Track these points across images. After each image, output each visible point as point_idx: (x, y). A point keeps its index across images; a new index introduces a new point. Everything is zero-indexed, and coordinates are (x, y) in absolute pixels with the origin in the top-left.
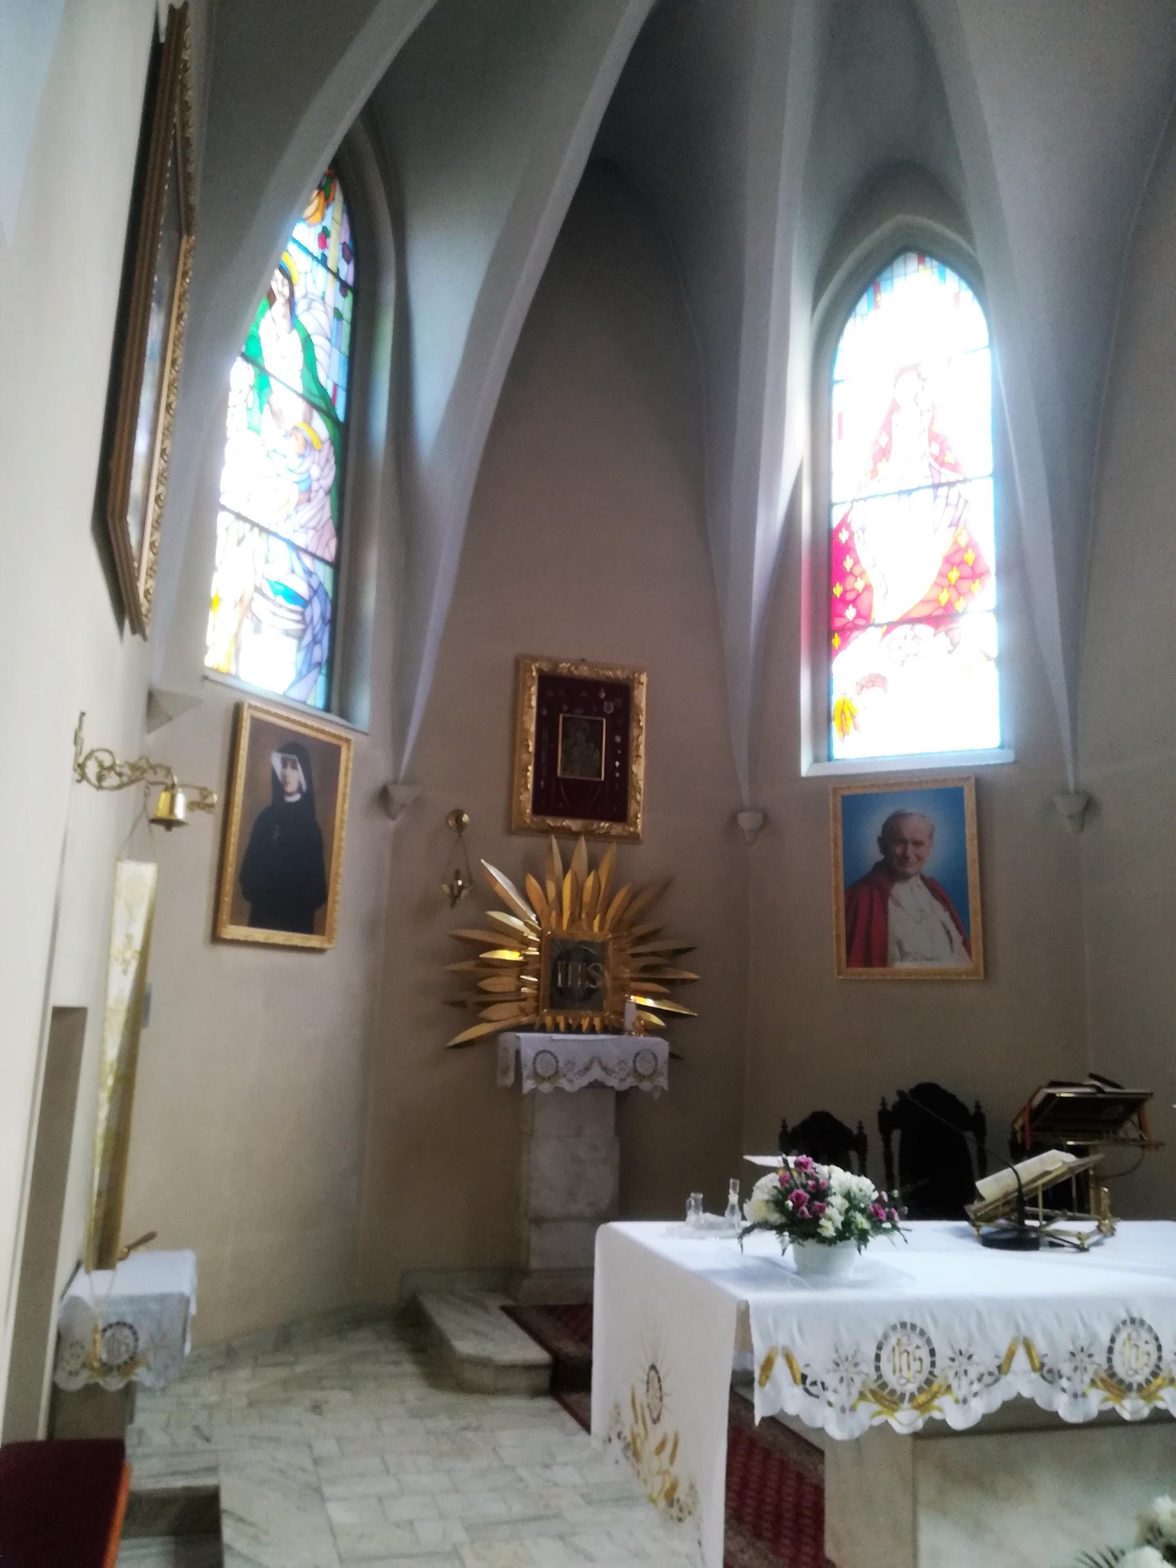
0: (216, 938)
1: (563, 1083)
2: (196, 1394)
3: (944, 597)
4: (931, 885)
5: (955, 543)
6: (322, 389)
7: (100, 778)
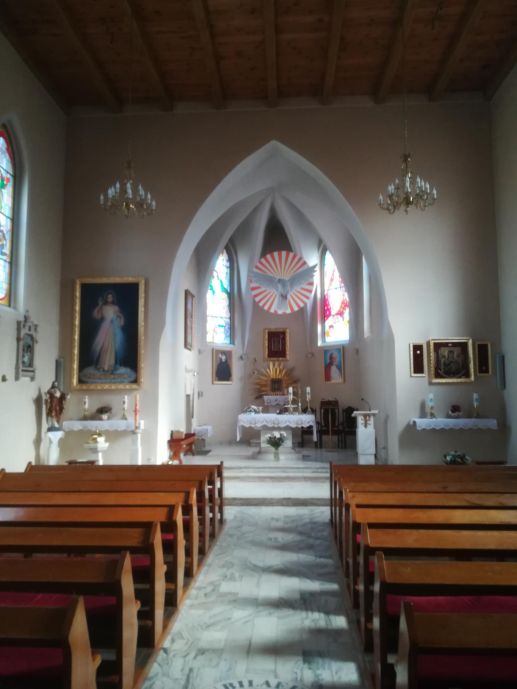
0: (213, 383)
1: (272, 404)
4: (336, 366)
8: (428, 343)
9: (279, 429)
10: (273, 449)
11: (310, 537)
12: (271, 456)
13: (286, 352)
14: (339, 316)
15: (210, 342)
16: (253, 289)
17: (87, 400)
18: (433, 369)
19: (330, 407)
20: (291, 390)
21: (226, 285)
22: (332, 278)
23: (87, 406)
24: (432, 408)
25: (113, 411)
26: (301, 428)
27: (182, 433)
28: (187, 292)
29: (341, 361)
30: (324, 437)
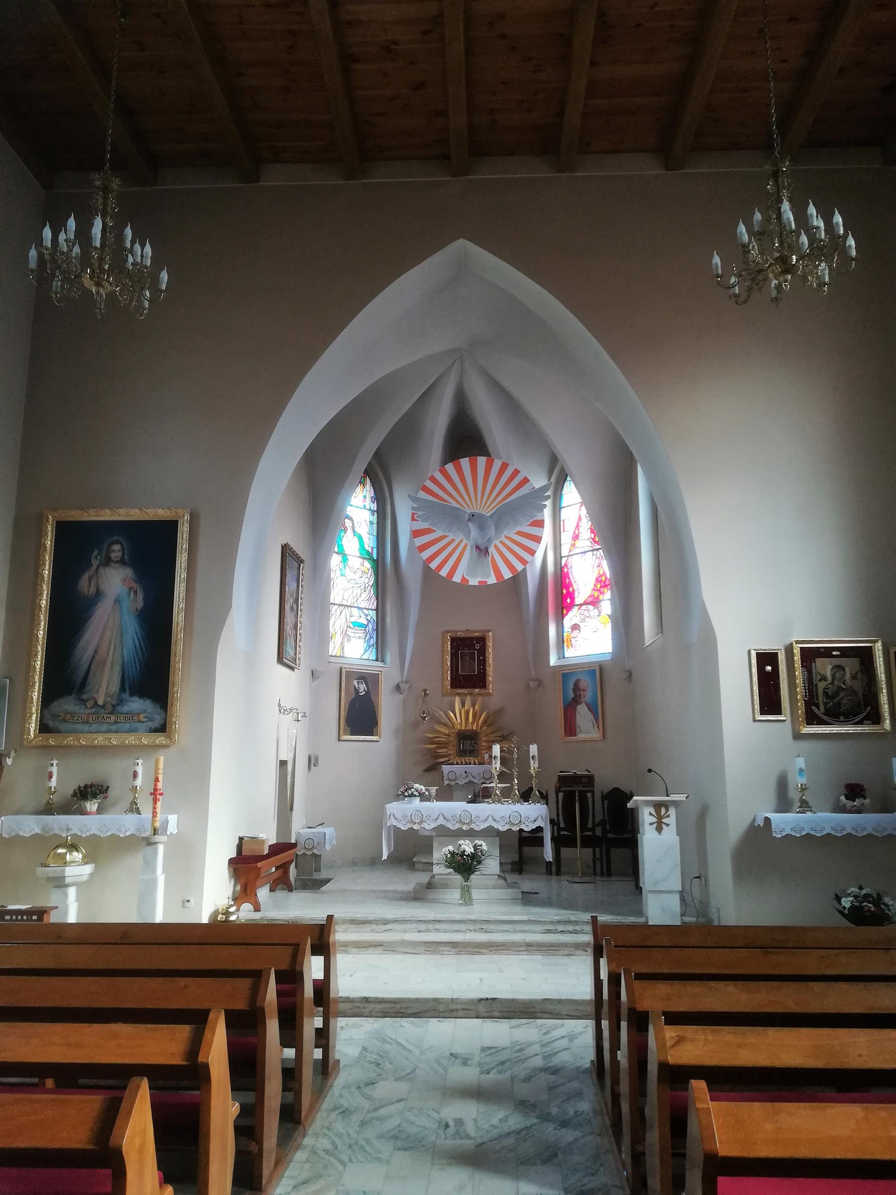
1: (458, 782)
3: (596, 594)
5: (599, 573)
7: (284, 712)
8: (789, 649)
9: (471, 834)
10: (458, 878)
11: (546, 1117)
12: (456, 894)
13: (487, 678)
14: (590, 607)
15: (335, 656)
16: (422, 548)
17: (54, 769)
18: (801, 704)
19: (577, 788)
20: (496, 749)
21: (370, 542)
22: (577, 532)
23: (53, 783)
24: (803, 789)
25: (112, 793)
26: (518, 833)
27: (263, 842)
28: (285, 549)
29: (596, 700)
30: (565, 852)
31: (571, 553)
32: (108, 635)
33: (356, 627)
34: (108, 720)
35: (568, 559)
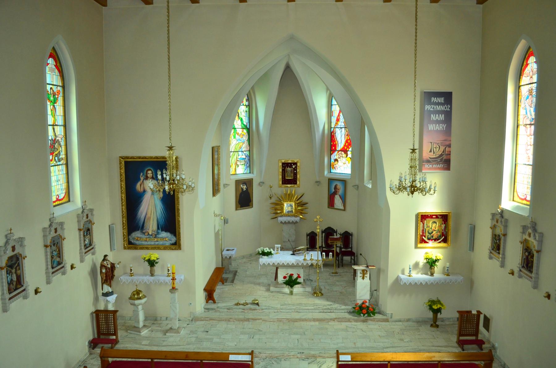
2: (239, 261)
6: (245, 125)
21: (246, 121)
22: (338, 118)
31: (336, 127)
32: (150, 207)
33: (241, 160)
34: (154, 240)
35: (334, 129)
